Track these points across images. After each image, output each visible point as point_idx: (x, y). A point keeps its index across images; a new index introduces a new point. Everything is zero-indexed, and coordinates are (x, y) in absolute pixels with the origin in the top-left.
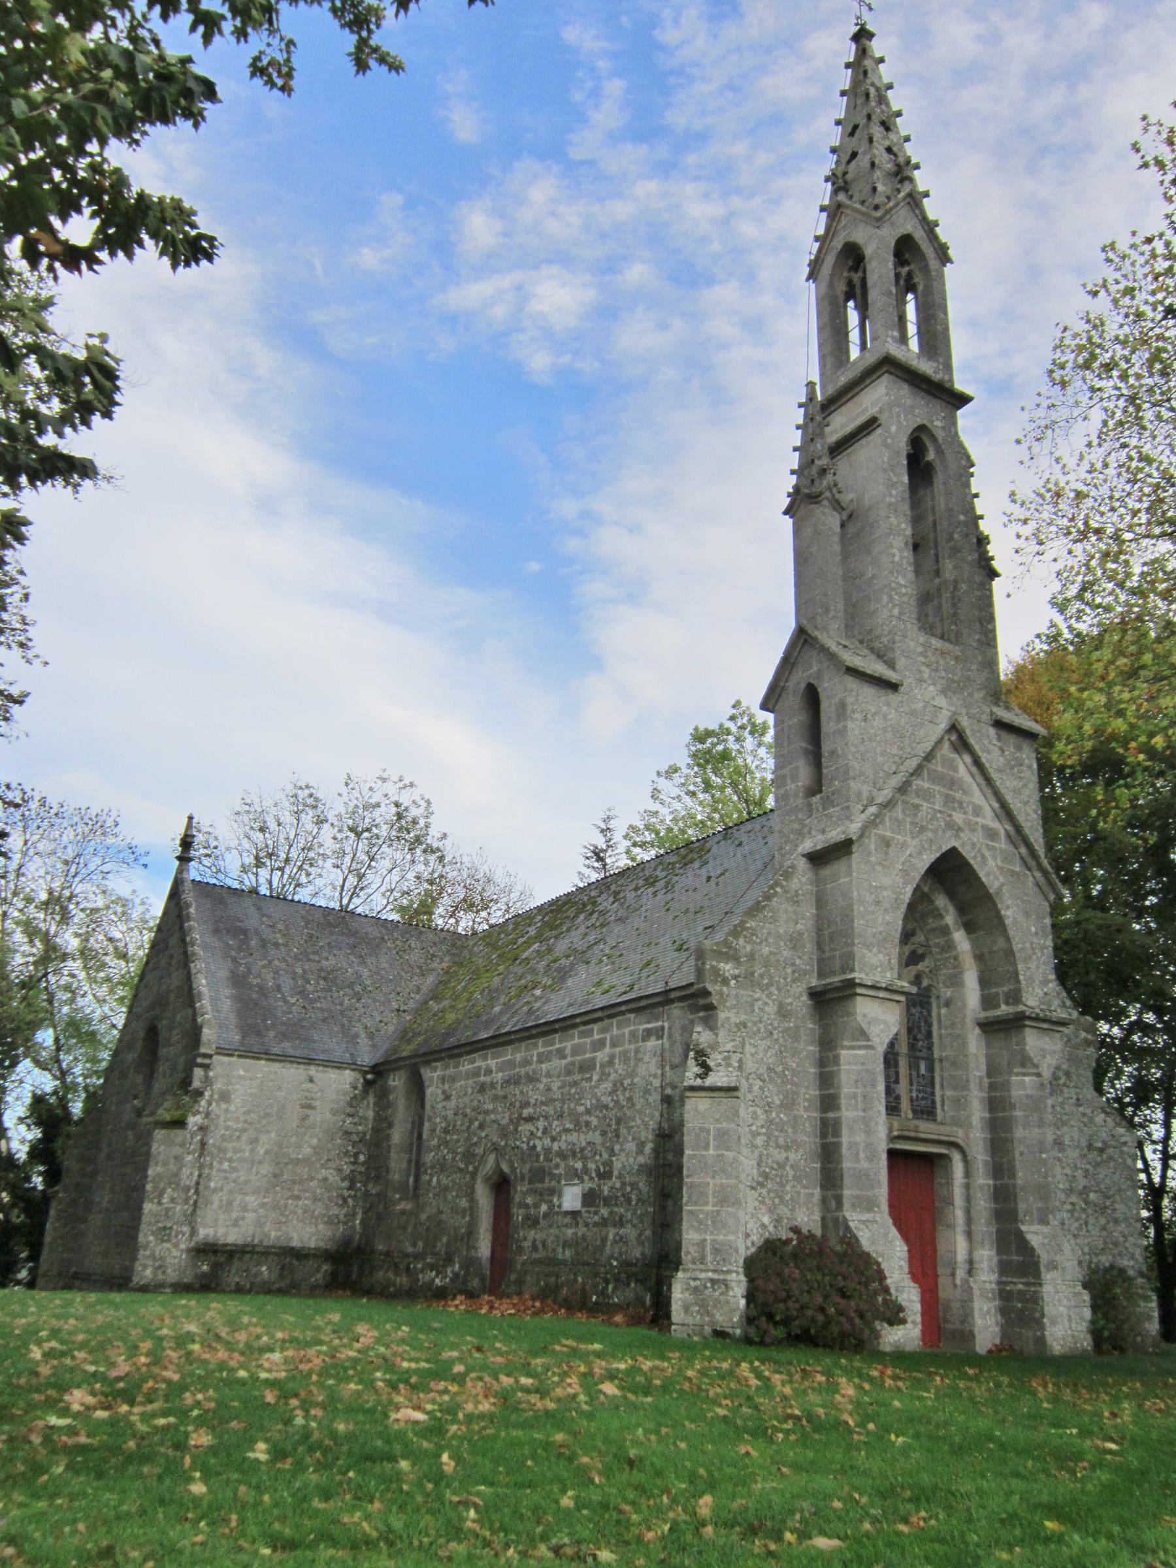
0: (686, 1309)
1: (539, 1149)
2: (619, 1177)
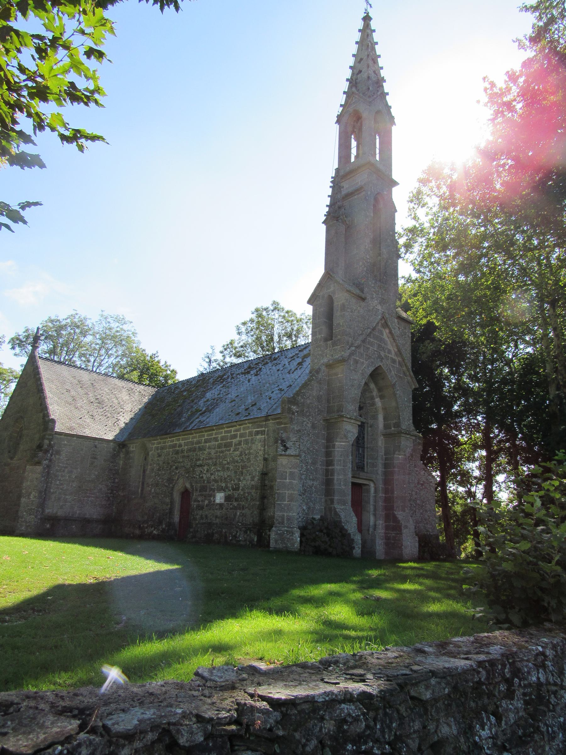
0: (276, 541)
1: (204, 478)
2: (242, 490)
